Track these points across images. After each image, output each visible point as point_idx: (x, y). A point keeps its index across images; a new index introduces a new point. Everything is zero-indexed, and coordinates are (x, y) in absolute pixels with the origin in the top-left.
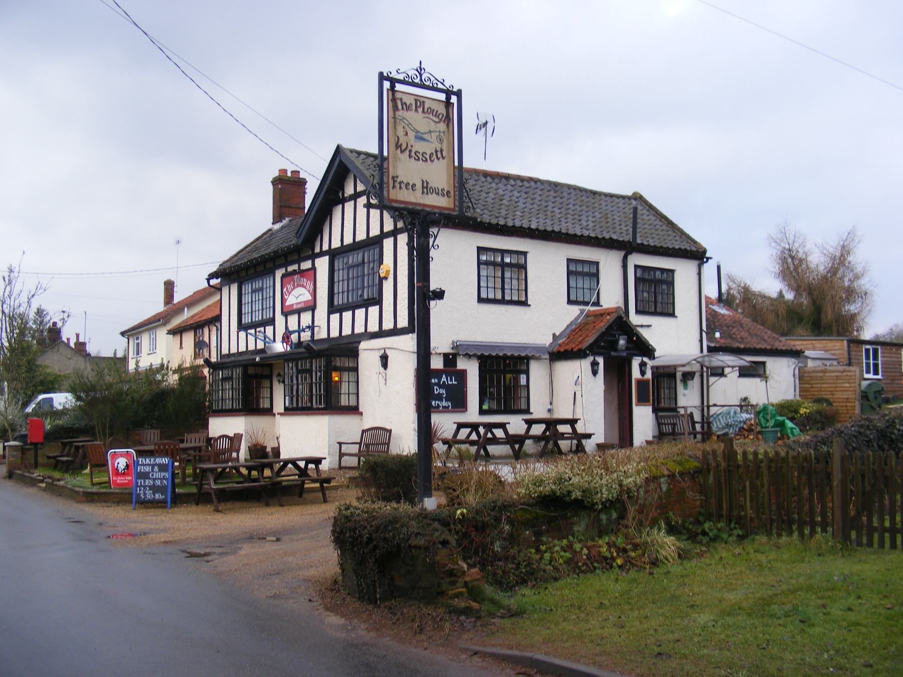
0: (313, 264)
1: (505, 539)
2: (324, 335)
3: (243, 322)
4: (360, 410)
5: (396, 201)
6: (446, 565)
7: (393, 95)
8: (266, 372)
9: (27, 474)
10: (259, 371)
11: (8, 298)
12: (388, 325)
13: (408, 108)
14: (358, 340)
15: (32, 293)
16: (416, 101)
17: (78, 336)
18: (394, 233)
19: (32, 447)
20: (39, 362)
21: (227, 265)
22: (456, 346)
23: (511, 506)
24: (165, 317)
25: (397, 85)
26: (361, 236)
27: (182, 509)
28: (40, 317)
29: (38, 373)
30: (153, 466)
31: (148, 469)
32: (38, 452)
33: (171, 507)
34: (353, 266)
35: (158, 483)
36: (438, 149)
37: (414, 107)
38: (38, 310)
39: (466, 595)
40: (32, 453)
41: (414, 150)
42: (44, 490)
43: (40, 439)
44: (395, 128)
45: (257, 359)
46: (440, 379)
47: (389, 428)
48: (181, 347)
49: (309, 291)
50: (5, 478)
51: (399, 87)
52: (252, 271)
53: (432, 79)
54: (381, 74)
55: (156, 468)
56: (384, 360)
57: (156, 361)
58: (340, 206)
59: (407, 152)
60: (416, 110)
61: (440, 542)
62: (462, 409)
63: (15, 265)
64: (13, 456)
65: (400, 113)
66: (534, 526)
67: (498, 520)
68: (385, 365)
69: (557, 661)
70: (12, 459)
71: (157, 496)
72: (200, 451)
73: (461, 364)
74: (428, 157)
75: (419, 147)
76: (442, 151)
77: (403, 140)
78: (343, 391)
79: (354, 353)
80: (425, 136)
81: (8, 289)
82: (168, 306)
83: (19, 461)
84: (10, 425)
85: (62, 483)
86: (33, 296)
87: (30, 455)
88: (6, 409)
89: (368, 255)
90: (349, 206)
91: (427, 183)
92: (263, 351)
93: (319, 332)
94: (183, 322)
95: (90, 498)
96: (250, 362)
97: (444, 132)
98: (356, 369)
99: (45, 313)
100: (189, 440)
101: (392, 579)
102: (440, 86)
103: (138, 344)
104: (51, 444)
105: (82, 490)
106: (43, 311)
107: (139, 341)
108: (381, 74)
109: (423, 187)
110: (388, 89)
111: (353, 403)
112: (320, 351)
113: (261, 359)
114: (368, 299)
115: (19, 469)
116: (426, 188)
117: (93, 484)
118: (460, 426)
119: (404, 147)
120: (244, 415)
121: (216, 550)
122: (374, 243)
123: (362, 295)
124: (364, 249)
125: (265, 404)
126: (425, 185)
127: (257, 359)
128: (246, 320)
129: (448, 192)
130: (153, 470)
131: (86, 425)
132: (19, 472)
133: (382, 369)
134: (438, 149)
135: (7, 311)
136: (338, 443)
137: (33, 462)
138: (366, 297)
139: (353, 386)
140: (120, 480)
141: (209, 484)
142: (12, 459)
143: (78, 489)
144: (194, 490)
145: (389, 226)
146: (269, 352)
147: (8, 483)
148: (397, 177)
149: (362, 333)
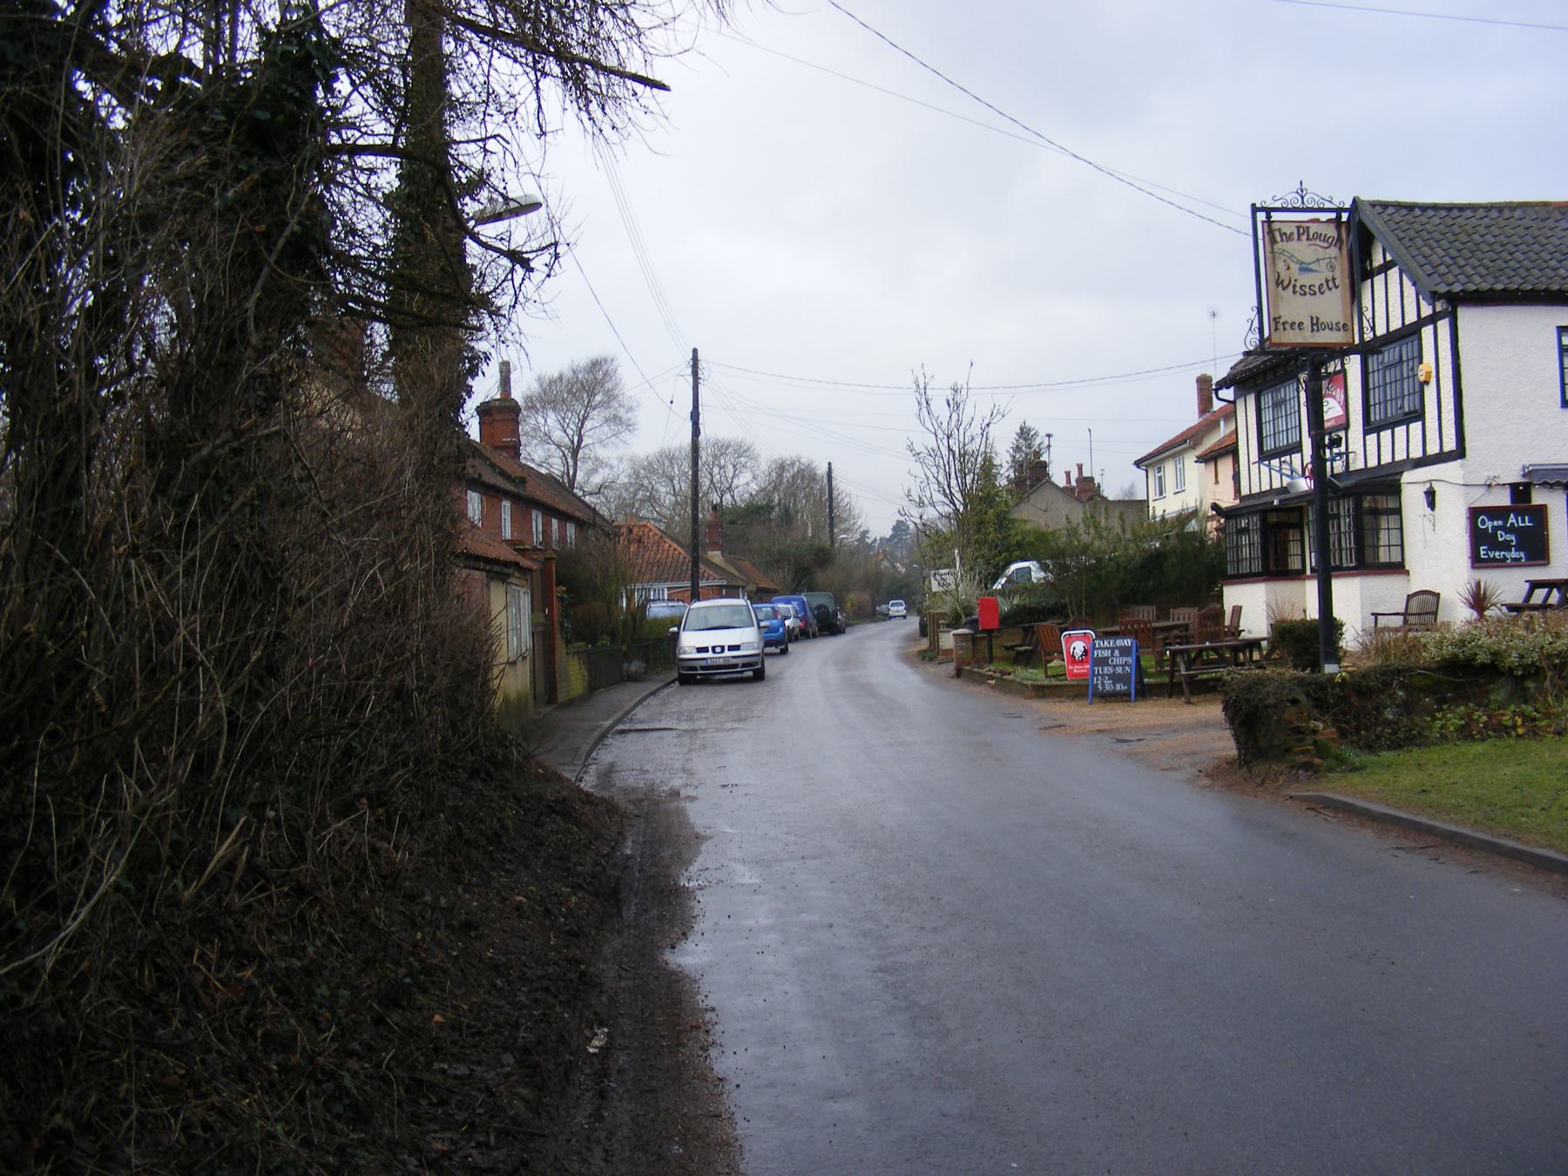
0: (1343, 365)
1: (1398, 706)
2: (1361, 465)
3: (1372, 419)
4: (1407, 568)
5: (1280, 345)
6: (1292, 722)
7: (1269, 226)
8: (1294, 518)
9: (976, 670)
10: (1283, 517)
11: (955, 429)
12: (1433, 449)
13: (1289, 238)
14: (1399, 470)
15: (986, 422)
16: (1298, 228)
17: (1080, 467)
18: (1433, 319)
19: (985, 635)
20: (1015, 515)
21: (1239, 368)
22: (1529, 473)
23: (1404, 671)
24: (1194, 435)
25: (1272, 214)
26: (1396, 324)
27: (1151, 702)
28: (1025, 439)
29: (1012, 532)
30: (1113, 650)
31: (1106, 653)
32: (994, 642)
33: (1136, 700)
34: (1389, 367)
35: (1119, 670)
36: (1330, 278)
37: (1296, 236)
38: (1022, 429)
39: (1314, 752)
40: (985, 643)
41: (1298, 285)
42: (993, 687)
43: (995, 625)
44: (1274, 263)
45: (1276, 503)
46: (1506, 519)
47: (1437, 591)
48: (1217, 482)
49: (1339, 403)
50: (953, 677)
51: (1275, 216)
52: (1270, 376)
53: (1317, 199)
54: (1253, 205)
55: (1117, 653)
56: (1431, 496)
57: (1189, 500)
58: (1369, 281)
59: (1291, 288)
60: (1299, 239)
61: (1289, 701)
62: (1541, 562)
63: (961, 382)
64: (962, 648)
65: (1279, 246)
66: (1435, 693)
67: (1387, 685)
68: (1432, 505)
69: (1338, 797)
70: (960, 652)
71: (1118, 687)
72: (1187, 630)
73: (1538, 498)
74: (1316, 289)
75: (1306, 279)
76: (1334, 279)
77: (1284, 276)
78: (1382, 543)
79: (1395, 489)
80: (1311, 266)
81: (955, 416)
82: (1204, 417)
83: (970, 655)
84: (964, 608)
85: (1011, 677)
86: (988, 425)
87: (983, 646)
88: (957, 586)
89: (1407, 350)
90: (1378, 280)
91: (1318, 319)
92: (1284, 490)
93: (1355, 460)
94: (1220, 441)
95: (1041, 692)
96: (1267, 506)
97: (1335, 258)
98: (1398, 511)
99: (1032, 433)
100: (1176, 617)
101: (1256, 741)
102: (1328, 205)
103: (1160, 478)
104: (1011, 630)
105: (1030, 682)
106: (1030, 430)
107: (1162, 473)
108: (1253, 205)
109: (1312, 325)
110: (1263, 222)
111: (1396, 558)
112: (1347, 488)
113: (1280, 501)
114: (1410, 413)
115: (969, 664)
116: (1316, 324)
117: (1047, 676)
118: (1535, 585)
119: (1285, 283)
120: (1264, 581)
121: (1148, 737)
122: (1410, 333)
123: (1402, 407)
124: (1401, 342)
125: (1295, 564)
126: (1315, 322)
127: (1276, 503)
128: (1269, 445)
129: (1345, 325)
130: (1112, 655)
131: (1056, 604)
132: (968, 668)
133: (1428, 510)
134: (1330, 278)
135: (956, 449)
136: (1373, 614)
137: (987, 655)
138: (1406, 409)
139: (1395, 534)
140: (1077, 669)
141: (1179, 671)
142: (960, 652)
143: (1026, 682)
144: (1166, 679)
145: (1426, 311)
146: (1293, 492)
147: (955, 682)
148: (1280, 317)
149: (1404, 460)
